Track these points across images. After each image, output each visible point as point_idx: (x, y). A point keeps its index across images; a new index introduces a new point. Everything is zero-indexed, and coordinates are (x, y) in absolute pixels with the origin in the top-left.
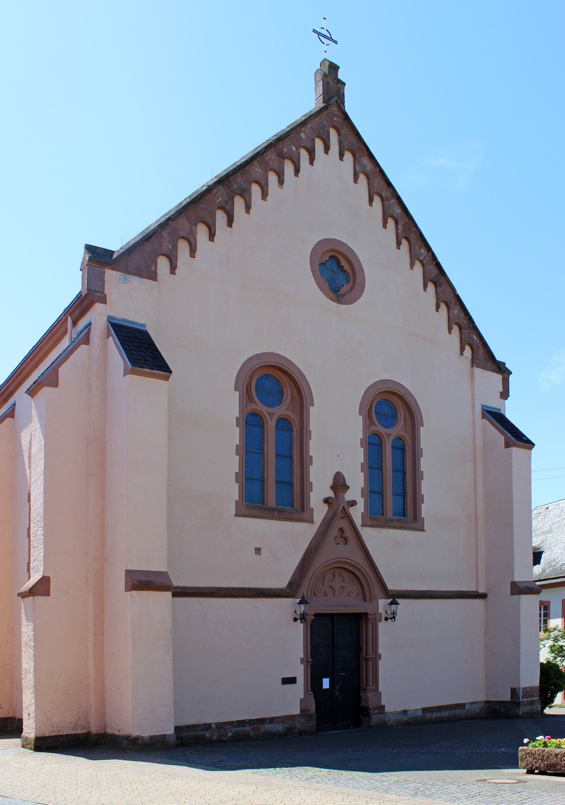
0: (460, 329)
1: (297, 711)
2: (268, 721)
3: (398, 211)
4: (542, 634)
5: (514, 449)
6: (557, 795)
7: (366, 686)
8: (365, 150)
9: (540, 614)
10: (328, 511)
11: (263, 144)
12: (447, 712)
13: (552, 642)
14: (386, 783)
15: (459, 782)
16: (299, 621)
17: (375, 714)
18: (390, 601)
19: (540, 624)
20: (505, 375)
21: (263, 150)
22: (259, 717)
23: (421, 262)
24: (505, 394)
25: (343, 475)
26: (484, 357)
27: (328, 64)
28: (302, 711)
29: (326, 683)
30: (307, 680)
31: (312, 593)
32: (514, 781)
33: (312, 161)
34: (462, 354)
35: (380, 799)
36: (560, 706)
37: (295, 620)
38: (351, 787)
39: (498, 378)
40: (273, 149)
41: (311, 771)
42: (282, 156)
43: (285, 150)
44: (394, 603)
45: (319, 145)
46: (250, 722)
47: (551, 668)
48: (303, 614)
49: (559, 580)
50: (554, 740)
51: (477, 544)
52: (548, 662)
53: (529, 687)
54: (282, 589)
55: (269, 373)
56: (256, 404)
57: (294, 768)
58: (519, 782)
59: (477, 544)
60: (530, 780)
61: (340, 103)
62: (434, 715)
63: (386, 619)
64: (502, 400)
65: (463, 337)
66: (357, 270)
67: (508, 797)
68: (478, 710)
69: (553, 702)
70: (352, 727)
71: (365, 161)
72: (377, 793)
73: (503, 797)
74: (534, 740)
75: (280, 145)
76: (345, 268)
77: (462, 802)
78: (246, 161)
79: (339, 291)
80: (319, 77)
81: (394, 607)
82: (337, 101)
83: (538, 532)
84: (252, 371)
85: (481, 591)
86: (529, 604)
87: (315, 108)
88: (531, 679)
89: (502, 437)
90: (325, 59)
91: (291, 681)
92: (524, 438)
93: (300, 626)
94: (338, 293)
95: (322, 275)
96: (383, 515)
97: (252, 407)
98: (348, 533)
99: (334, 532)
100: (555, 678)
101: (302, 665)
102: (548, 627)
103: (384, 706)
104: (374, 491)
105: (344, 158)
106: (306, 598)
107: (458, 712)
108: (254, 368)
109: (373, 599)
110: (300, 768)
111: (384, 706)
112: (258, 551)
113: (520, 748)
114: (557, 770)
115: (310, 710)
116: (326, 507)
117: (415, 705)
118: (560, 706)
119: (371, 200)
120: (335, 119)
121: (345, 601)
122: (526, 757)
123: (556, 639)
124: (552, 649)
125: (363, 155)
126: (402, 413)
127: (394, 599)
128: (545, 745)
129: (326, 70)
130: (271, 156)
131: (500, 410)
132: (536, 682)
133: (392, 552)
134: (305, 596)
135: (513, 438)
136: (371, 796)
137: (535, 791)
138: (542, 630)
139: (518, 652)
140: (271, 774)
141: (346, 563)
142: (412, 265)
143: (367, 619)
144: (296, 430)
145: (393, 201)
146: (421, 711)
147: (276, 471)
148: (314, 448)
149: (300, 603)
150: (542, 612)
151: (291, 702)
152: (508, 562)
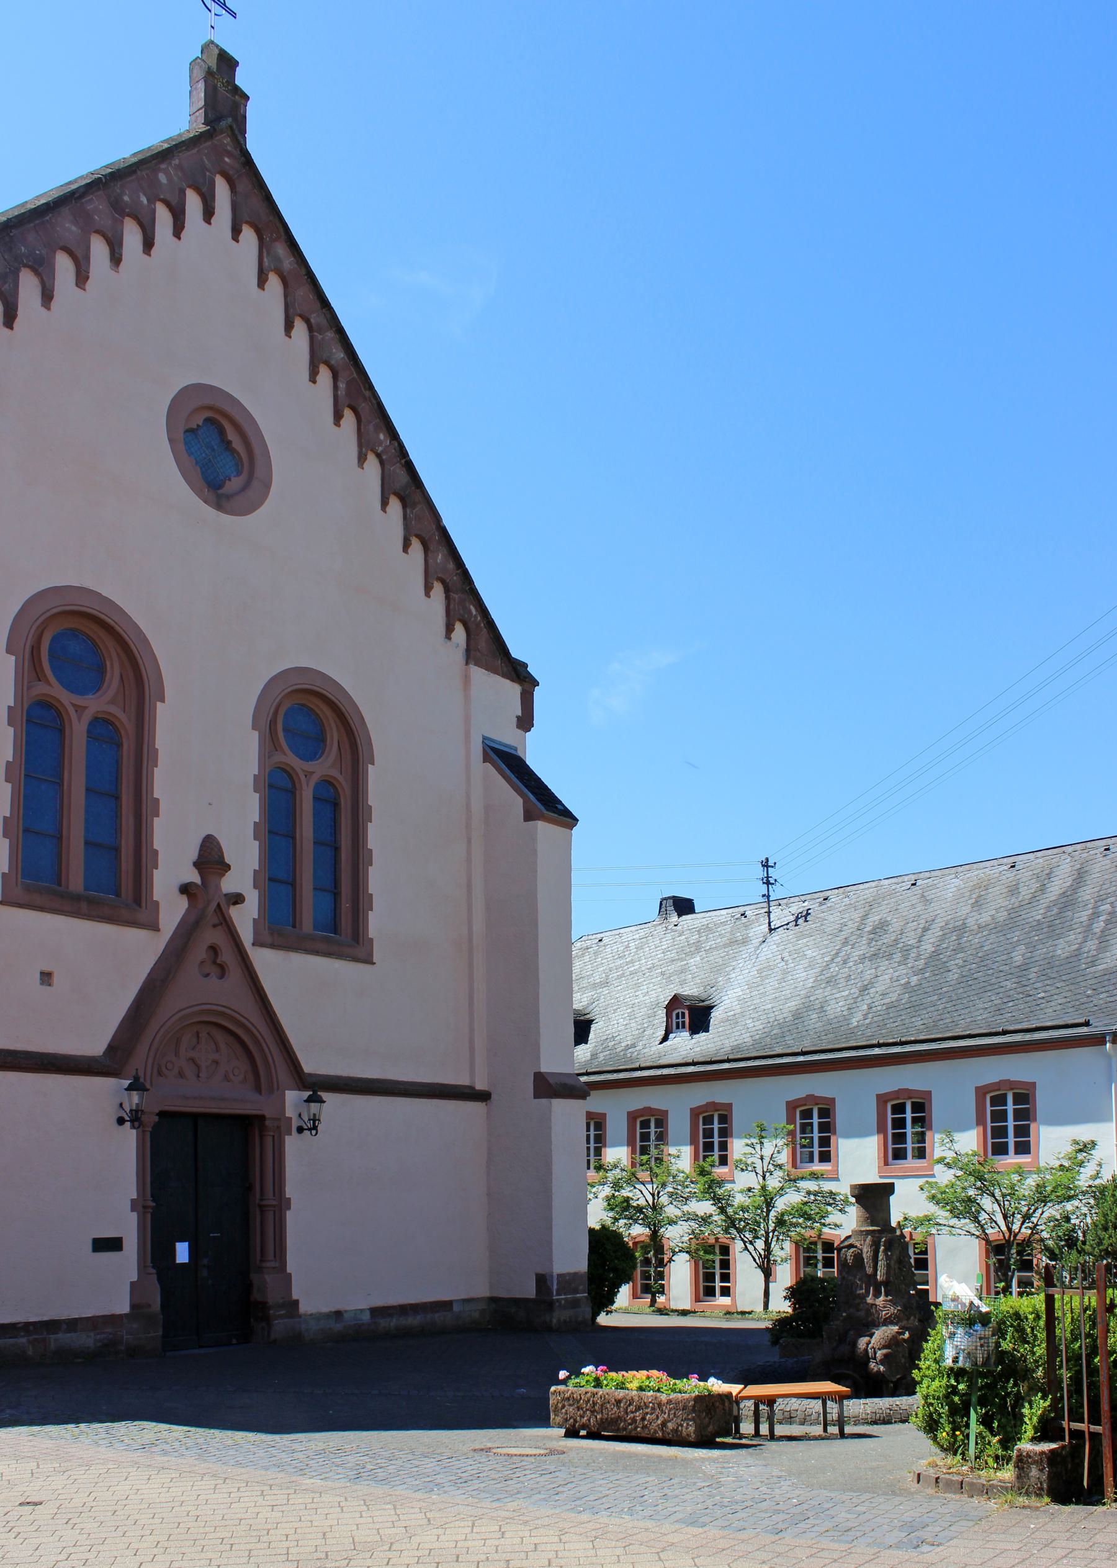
0: (447, 590)
1: (124, 1308)
2: (64, 1327)
3: (339, 355)
4: (592, 1174)
5: (540, 825)
6: (618, 1477)
7: (261, 1261)
8: (282, 230)
9: (588, 1137)
10: (188, 911)
11: (82, 177)
12: (419, 1317)
13: (609, 1189)
14: (301, 1455)
15: (440, 1454)
16: (128, 1124)
17: (280, 1317)
18: (307, 1094)
19: (588, 1155)
20: (526, 685)
21: (82, 190)
22: (46, 1318)
23: (378, 456)
24: (526, 722)
25: (218, 843)
26: (488, 648)
27: (216, 52)
28: (133, 1306)
29: (182, 1252)
30: (145, 1243)
31: (155, 1070)
32: (542, 1452)
33: (178, 229)
34: (448, 636)
35: (288, 1488)
36: (626, 1311)
37: (121, 1121)
38: (232, 1462)
39: (514, 690)
40: (100, 192)
41: (151, 1430)
42: (120, 210)
43: (126, 198)
44: (314, 1099)
45: (193, 203)
46: (28, 1328)
47: (608, 1239)
48: (137, 1111)
49: (622, 1076)
50: (613, 1374)
51: (471, 998)
52: (603, 1226)
53: (569, 1274)
54: (93, 1059)
55: (73, 626)
56: (50, 685)
57: (115, 1425)
58: (552, 1452)
59: (471, 998)
60: (571, 1449)
61: (236, 132)
62: (393, 1323)
63: (300, 1130)
64: (520, 732)
65: (452, 606)
66: (257, 450)
67: (531, 1482)
68: (476, 1315)
69: (612, 1302)
70: (234, 1341)
71: (281, 250)
72: (282, 1475)
73: (522, 1482)
74: (578, 1374)
75: (117, 188)
76: (234, 445)
77: (445, 1492)
78: (47, 204)
79: (220, 487)
80: (199, 74)
81: (314, 1107)
82: (231, 127)
83: (584, 983)
84: (42, 618)
85: (480, 1086)
86: (568, 1115)
87: (188, 131)
88: (572, 1259)
89: (520, 801)
90: (212, 42)
91: (108, 1245)
92: (560, 807)
93: (129, 1136)
94: (220, 492)
95: (190, 454)
96: (294, 926)
97: (41, 689)
98: (227, 956)
99: (199, 953)
100: (617, 1258)
101: (135, 1214)
102: (603, 1162)
103: (297, 1302)
104: (277, 878)
105: (241, 237)
106: (142, 1080)
107: (438, 1317)
108: (48, 614)
109: (275, 1090)
110: (129, 1423)
111: (297, 1302)
112: (46, 977)
113: (553, 1388)
114: (618, 1430)
115: (150, 1306)
116: (183, 903)
117: (358, 1300)
118: (626, 1311)
119: (289, 327)
120: (227, 159)
121: (220, 1090)
122: (563, 1407)
123: (617, 1186)
124: (611, 1204)
125: (275, 240)
126: (334, 734)
127: (315, 1092)
128: (598, 1383)
129: (213, 63)
130: (97, 204)
131: (516, 750)
132: (581, 1265)
133: (310, 998)
134: (141, 1074)
135: (538, 804)
136: (271, 1482)
137: (580, 1471)
138: (592, 1167)
139: (548, 1206)
140: (68, 1436)
141: (223, 1014)
142: (362, 459)
143: (263, 1129)
144: (128, 745)
145: (330, 335)
146: (368, 1314)
147: (87, 821)
148: (163, 783)
149: (130, 1088)
150: (592, 1133)
151: (110, 1288)
152: (528, 1032)
